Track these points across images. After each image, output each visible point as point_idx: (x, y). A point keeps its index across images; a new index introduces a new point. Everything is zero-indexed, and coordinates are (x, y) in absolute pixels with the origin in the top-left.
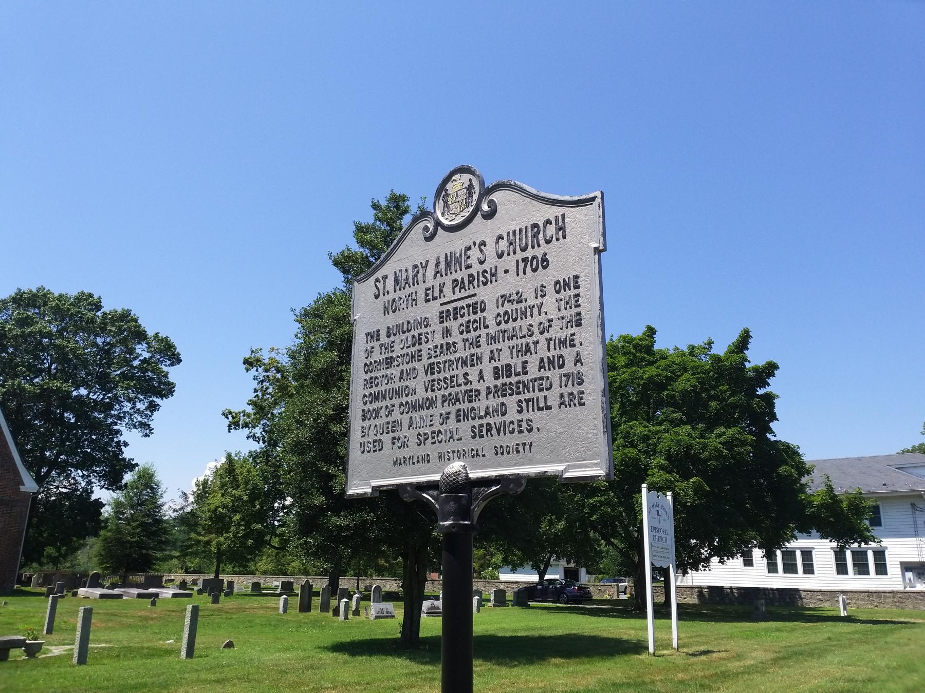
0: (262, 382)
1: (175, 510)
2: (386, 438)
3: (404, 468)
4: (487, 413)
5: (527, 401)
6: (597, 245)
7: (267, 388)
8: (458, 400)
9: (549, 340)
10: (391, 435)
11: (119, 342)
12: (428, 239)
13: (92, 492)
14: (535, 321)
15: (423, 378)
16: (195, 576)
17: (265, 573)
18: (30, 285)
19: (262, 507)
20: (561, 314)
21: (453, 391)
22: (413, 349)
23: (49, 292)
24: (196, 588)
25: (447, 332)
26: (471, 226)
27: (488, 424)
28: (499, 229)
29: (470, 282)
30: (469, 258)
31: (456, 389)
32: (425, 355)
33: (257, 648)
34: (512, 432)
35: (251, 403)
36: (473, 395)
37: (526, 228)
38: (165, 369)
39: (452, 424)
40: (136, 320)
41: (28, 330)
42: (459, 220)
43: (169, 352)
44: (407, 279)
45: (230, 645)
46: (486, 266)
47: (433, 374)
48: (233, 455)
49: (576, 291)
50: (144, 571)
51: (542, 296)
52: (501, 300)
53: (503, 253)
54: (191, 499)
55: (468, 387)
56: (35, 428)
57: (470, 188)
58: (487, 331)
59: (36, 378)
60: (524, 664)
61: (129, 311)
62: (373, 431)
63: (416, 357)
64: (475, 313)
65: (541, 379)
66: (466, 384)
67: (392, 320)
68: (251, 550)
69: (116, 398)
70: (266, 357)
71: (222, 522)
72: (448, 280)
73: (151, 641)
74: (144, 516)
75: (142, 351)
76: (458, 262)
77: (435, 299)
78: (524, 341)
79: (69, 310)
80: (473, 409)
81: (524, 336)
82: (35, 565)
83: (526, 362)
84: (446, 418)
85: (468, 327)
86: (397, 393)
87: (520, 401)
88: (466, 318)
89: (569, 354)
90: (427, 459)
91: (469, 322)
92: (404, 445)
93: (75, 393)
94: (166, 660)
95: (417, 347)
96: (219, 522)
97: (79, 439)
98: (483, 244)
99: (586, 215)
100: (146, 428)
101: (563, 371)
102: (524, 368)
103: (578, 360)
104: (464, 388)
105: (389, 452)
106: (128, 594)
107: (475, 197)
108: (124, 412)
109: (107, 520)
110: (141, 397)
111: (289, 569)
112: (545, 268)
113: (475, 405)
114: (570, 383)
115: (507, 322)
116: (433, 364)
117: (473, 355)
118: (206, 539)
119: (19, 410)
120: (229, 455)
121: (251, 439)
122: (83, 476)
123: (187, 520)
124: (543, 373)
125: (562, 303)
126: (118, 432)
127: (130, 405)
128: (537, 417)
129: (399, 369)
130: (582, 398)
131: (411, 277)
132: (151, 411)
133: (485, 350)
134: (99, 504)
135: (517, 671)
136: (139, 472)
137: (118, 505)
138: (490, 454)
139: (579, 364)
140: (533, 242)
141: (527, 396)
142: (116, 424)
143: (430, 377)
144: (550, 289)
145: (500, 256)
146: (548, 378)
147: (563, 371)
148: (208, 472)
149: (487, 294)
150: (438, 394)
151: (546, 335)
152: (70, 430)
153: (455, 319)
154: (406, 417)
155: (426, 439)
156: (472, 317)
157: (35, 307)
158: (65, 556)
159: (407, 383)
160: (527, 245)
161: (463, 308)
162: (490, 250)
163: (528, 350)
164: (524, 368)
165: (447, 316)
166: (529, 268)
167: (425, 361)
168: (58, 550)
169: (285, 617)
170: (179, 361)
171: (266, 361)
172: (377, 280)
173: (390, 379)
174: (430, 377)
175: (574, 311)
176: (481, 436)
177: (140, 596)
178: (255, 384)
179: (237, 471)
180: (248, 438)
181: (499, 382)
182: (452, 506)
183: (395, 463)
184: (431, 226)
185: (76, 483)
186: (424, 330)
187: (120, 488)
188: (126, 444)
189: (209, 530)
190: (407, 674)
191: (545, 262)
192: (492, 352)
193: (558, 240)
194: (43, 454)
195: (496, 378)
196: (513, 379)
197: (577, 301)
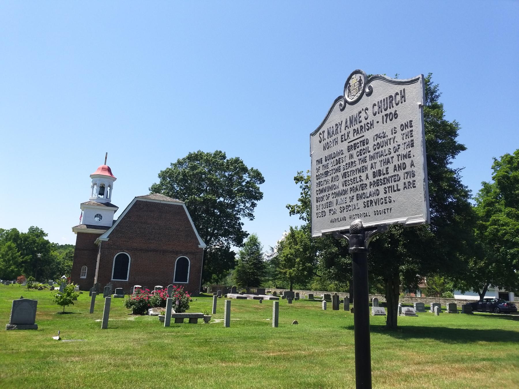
0: (304, 189)
1: (268, 256)
2: (327, 210)
3: (335, 224)
4: (370, 195)
5: (389, 187)
6: (420, 103)
7: (307, 192)
8: (357, 190)
9: (398, 156)
10: (329, 208)
11: (235, 174)
12: (342, 110)
13: (230, 248)
14: (391, 146)
15: (341, 180)
16: (281, 290)
17: (316, 290)
18: (194, 150)
19: (310, 255)
20: (404, 142)
21: (355, 185)
22: (336, 167)
23: (203, 153)
24: (281, 296)
25: (351, 156)
27: (371, 200)
28: (374, 100)
29: (361, 130)
30: (360, 117)
31: (356, 184)
32: (342, 169)
33: (309, 325)
34: (382, 204)
35: (300, 200)
36: (363, 187)
37: (387, 98)
38: (258, 186)
39: (355, 201)
40: (242, 162)
41: (195, 172)
42: (355, 98)
43: (258, 177)
44: (333, 131)
45: (296, 323)
46: (368, 121)
47: (345, 178)
48: (294, 228)
49: (411, 129)
50: (257, 287)
51: (395, 133)
52: (375, 137)
53: (376, 112)
54: (275, 251)
55: (362, 183)
56: (203, 218)
57: (361, 80)
58: (369, 154)
59: (201, 194)
60: (461, 343)
61: (238, 158)
62: (321, 207)
63: (338, 170)
64: (364, 145)
65: (395, 176)
66: (360, 181)
67: (327, 153)
68: (307, 277)
69: (236, 201)
70: (305, 175)
71: (291, 262)
72: (351, 130)
73: (259, 319)
74: (254, 260)
75: (246, 177)
76: (356, 120)
77: (345, 140)
78: (387, 157)
79: (212, 160)
80: (364, 193)
81: (387, 155)
82: (208, 283)
83: (388, 168)
84: (352, 199)
85: (361, 153)
86: (330, 188)
87: (385, 188)
88: (360, 148)
90: (344, 219)
91: (361, 150)
92: (334, 213)
93: (218, 201)
94: (265, 327)
95: (339, 165)
96: (289, 262)
97: (222, 223)
98: (367, 109)
99: (415, 88)
100: (251, 216)
101: (406, 171)
102: (387, 171)
103: (412, 165)
104: (359, 183)
105: (329, 217)
106: (250, 297)
107: (363, 85)
108: (241, 209)
109: (237, 261)
110: (248, 200)
111: (329, 288)
112: (396, 118)
113: (365, 191)
114: (409, 176)
115: (378, 148)
116: (346, 173)
117: (363, 167)
118: (284, 271)
120: (291, 228)
121: (302, 219)
122: (225, 240)
123: (275, 262)
124: (396, 173)
125: (404, 136)
126: (239, 218)
127: (243, 205)
129: (331, 177)
130: (414, 184)
131: (335, 130)
132: (253, 207)
133: (369, 163)
134: (233, 254)
135: (453, 346)
136: (250, 237)
137: (242, 254)
138: (372, 215)
139: (413, 167)
140: (390, 105)
141: (389, 185)
142: (237, 214)
143: (344, 179)
144: (398, 129)
145: (375, 115)
146: (398, 175)
147: (406, 171)
148: (283, 237)
149: (369, 135)
150: (349, 187)
151: (397, 153)
152: (218, 218)
153: (355, 149)
154: (335, 199)
155: (344, 210)
156: (362, 147)
157: (197, 160)
158: (221, 279)
159: (335, 183)
160: (387, 107)
161: (358, 143)
162: (370, 112)
163: (389, 162)
164: (387, 171)
165: (351, 148)
166: (388, 119)
167: (342, 172)
168: (218, 276)
169: (325, 312)
170: (264, 181)
171: (306, 178)
172: (320, 134)
173: (327, 182)
174: (344, 179)
175: (410, 139)
176: (368, 207)
177: (255, 298)
178: (301, 190)
179: (296, 236)
180: (300, 219)
181: (375, 179)
182: (355, 240)
183: (331, 222)
184: (343, 103)
185: (223, 243)
186: (341, 156)
187: (242, 246)
188: (243, 224)
189: (285, 266)
190: (387, 343)
191: (396, 115)
192: (372, 164)
193: (402, 103)
194: (207, 230)
195: (374, 177)
196: (382, 177)
197: (412, 134)
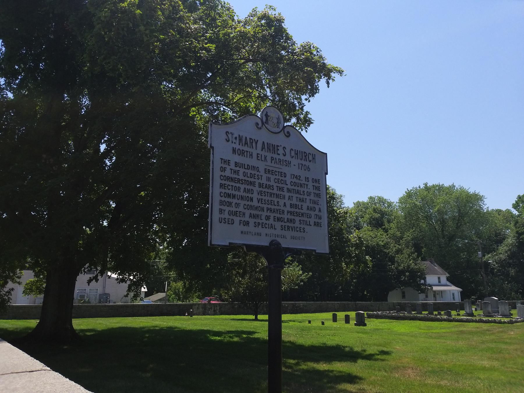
5: (303, 221)
26: (279, 134)
89: (317, 207)
119: (38, 288)
128: (307, 228)
